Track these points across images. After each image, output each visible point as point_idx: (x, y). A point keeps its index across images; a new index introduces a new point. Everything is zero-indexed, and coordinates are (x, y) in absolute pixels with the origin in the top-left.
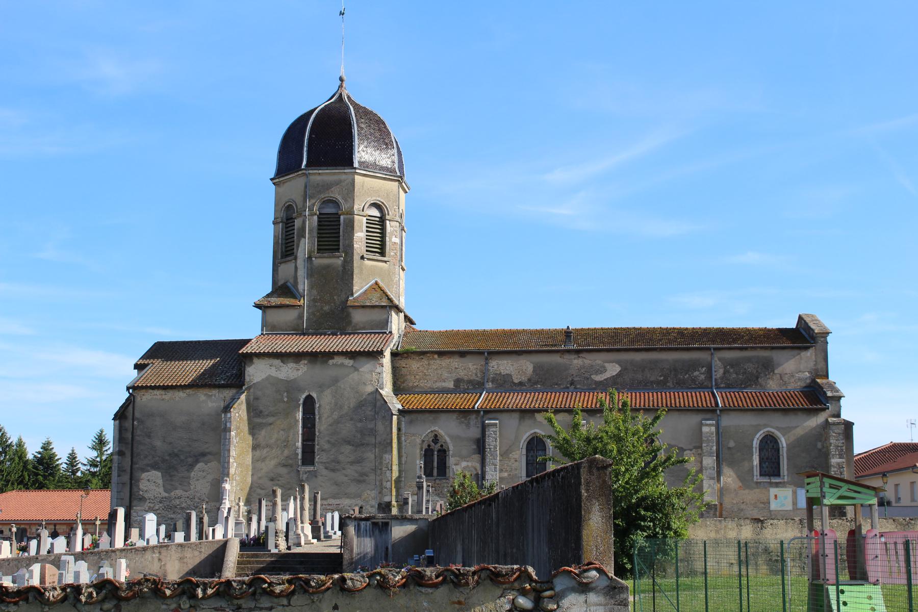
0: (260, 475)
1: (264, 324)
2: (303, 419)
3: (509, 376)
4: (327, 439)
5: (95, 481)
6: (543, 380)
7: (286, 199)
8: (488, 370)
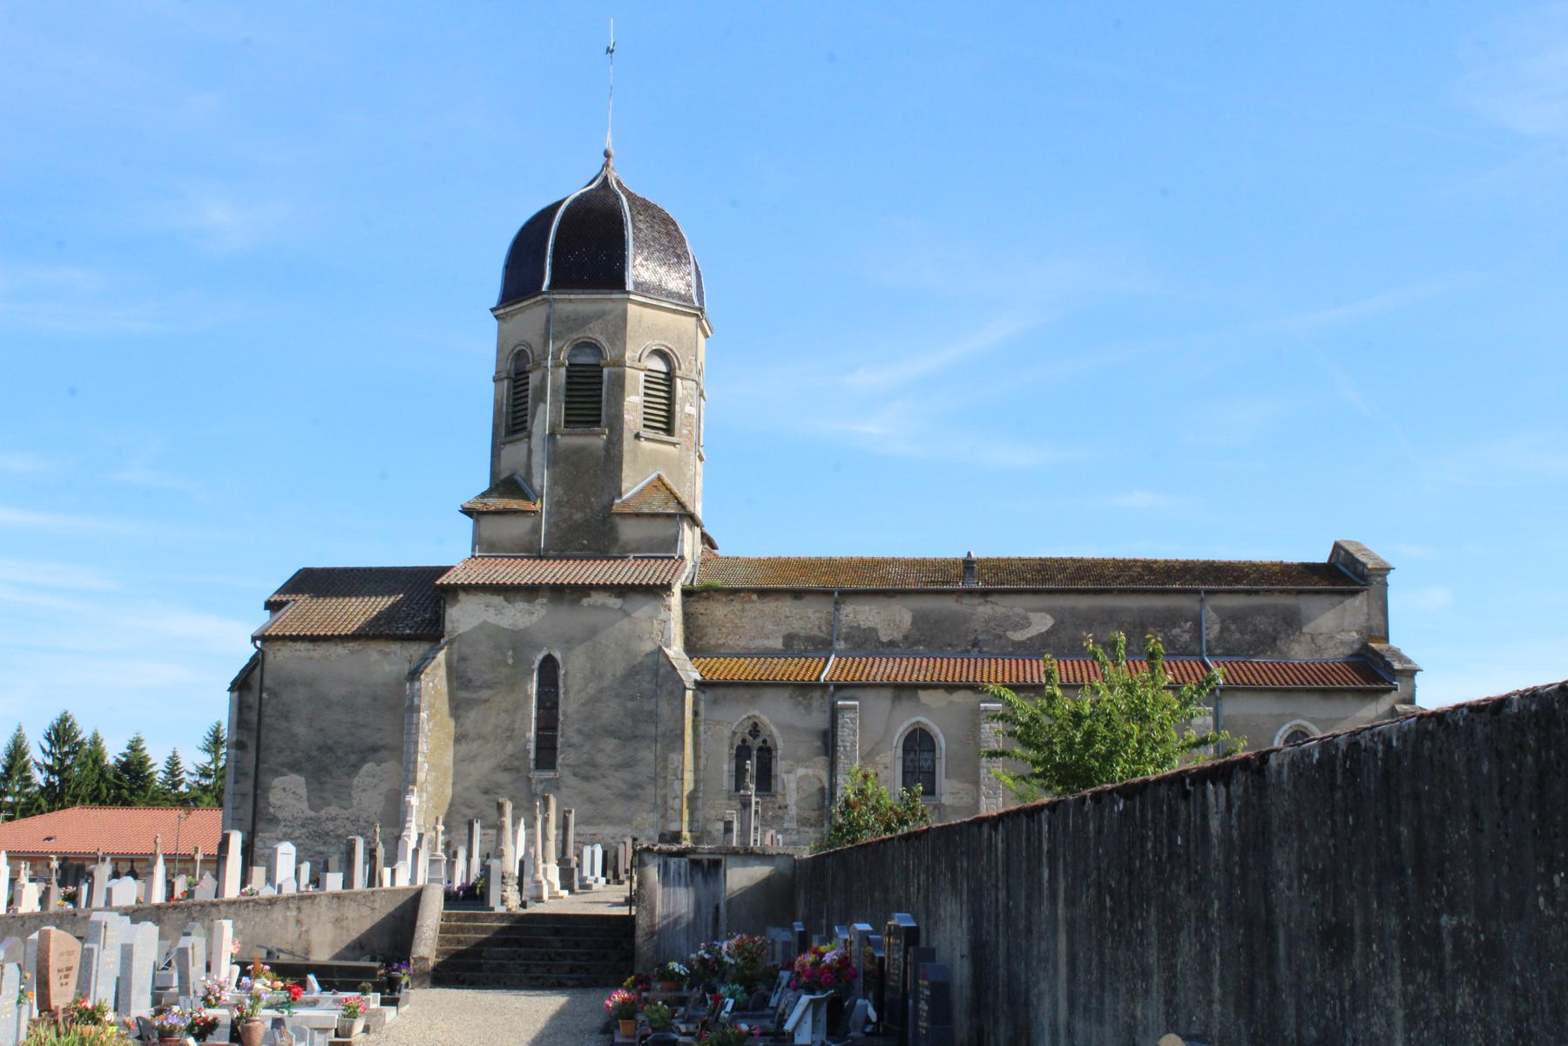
1: (477, 541)
2: (539, 694)
3: (874, 630)
5: (206, 799)
6: (927, 637)
8: (839, 621)
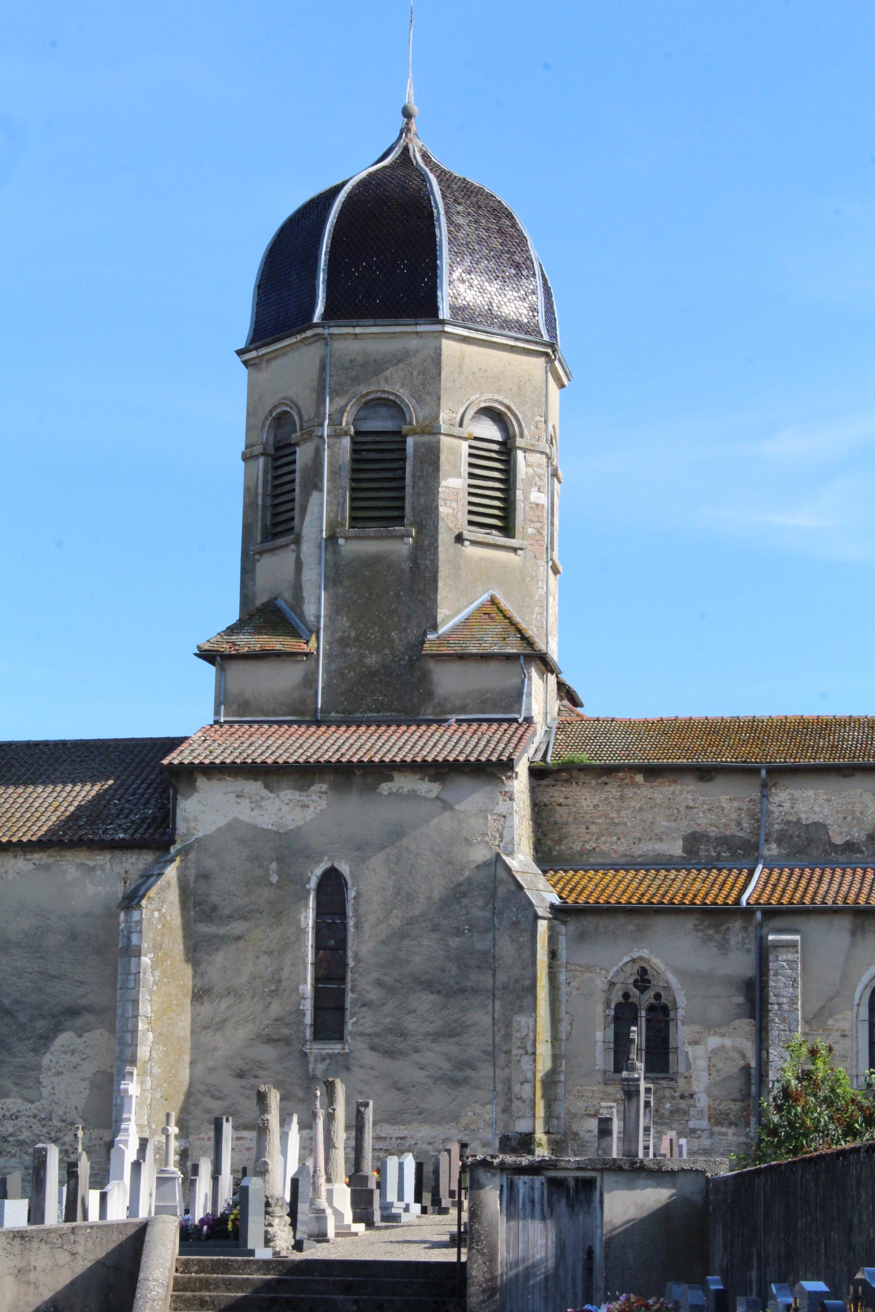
0: (211, 1063)
1: (222, 699)
2: (318, 927)
3: (821, 827)
4: (375, 975)
7: (275, 400)
8: (769, 813)
